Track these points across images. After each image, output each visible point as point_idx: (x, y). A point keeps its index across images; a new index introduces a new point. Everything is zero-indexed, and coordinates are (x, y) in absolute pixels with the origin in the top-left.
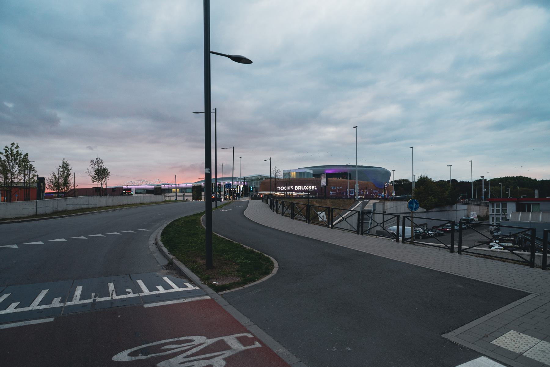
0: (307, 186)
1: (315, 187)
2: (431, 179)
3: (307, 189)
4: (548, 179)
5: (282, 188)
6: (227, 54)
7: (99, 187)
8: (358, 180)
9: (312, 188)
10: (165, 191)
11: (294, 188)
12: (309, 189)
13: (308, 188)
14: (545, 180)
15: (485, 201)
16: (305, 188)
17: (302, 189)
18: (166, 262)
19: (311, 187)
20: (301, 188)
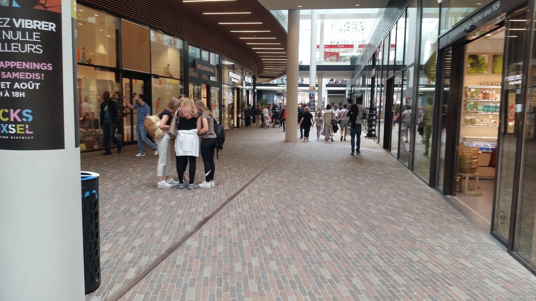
3: (7, 132)
5: (24, 86)
9: (18, 129)
12: (10, 132)
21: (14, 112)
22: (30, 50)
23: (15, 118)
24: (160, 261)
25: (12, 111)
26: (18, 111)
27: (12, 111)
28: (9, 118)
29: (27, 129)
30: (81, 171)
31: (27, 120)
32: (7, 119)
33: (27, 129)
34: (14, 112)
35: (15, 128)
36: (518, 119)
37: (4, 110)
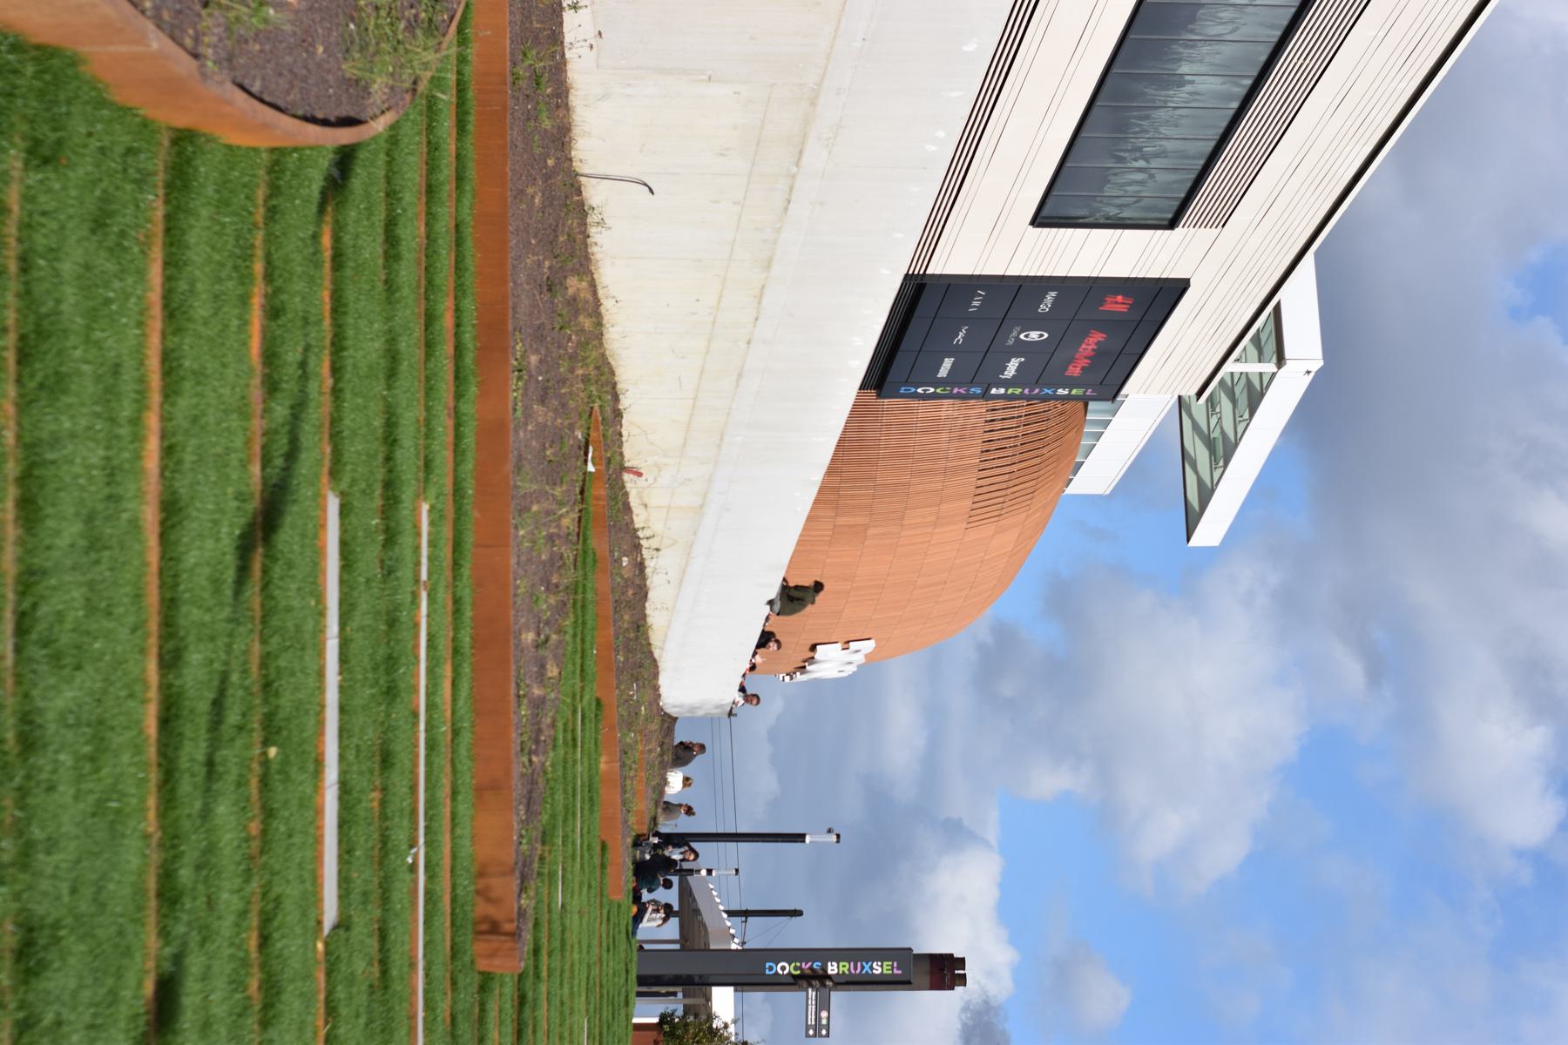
0: (864, 972)
9: (885, 967)
20: (849, 970)
26: (809, 964)
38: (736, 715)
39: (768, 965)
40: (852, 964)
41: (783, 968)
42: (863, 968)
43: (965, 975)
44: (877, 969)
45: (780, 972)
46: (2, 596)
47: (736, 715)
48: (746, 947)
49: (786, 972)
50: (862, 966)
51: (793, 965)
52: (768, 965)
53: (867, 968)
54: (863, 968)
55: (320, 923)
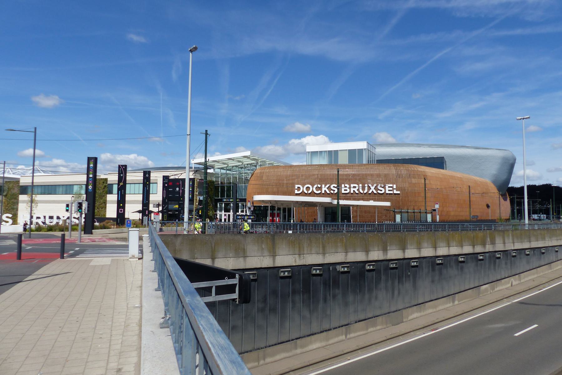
0: (90, 181)
1: (395, 187)
2: (548, 184)
3: (375, 192)
4: (555, 184)
5: (308, 188)
6: (179, 293)
7: (127, 174)
8: (531, 209)
9: (387, 189)
10: (41, 193)
11: (339, 188)
12: (379, 192)
13: (376, 188)
14: (520, 187)
15: (517, 201)
16: (369, 188)
17: (362, 192)
18: (138, 259)
19: (384, 187)
20: (358, 190)
21: (325, 186)
22: (217, 294)
23: (325, 191)
24: (326, 265)
25: (323, 186)
26: (328, 185)
27: (323, 186)
28: (321, 190)
29: (395, 189)
30: (288, 208)
31: (334, 192)
32: (319, 192)
33: (395, 189)
34: (325, 186)
35: (384, 187)
36: (4, 185)
37: (308, 192)
38: (159, 203)
39: (297, 186)
40: (361, 185)
41: (90, 187)
42: (91, 169)
43: (529, 187)
44: (92, 165)
45: (91, 188)
46: (561, 209)
47: (159, 203)
48: (189, 233)
49: (91, 187)
50: (369, 187)
51: (316, 186)
52: (297, 186)
53: (91, 168)
54: (91, 169)
55: (179, 283)
